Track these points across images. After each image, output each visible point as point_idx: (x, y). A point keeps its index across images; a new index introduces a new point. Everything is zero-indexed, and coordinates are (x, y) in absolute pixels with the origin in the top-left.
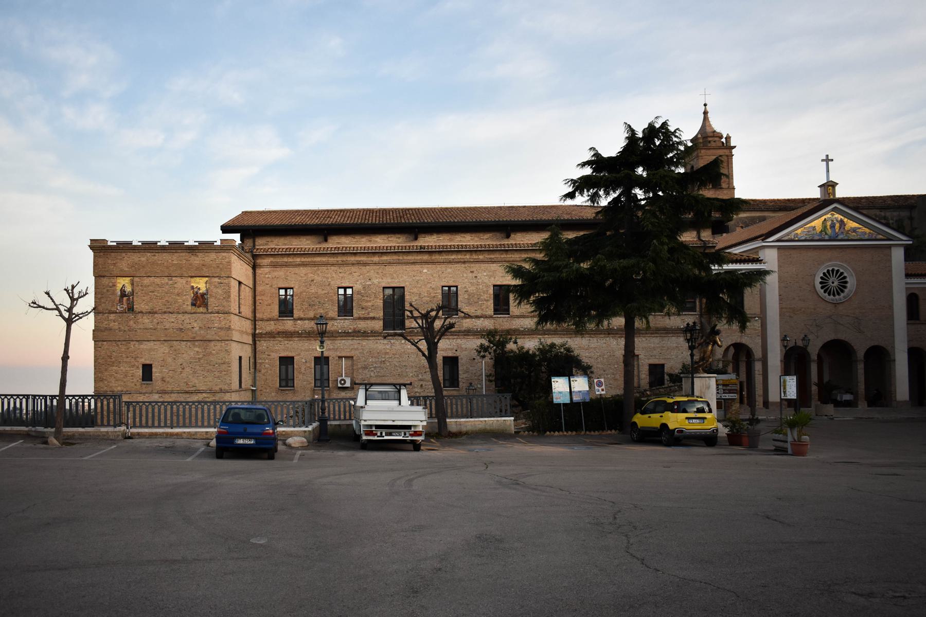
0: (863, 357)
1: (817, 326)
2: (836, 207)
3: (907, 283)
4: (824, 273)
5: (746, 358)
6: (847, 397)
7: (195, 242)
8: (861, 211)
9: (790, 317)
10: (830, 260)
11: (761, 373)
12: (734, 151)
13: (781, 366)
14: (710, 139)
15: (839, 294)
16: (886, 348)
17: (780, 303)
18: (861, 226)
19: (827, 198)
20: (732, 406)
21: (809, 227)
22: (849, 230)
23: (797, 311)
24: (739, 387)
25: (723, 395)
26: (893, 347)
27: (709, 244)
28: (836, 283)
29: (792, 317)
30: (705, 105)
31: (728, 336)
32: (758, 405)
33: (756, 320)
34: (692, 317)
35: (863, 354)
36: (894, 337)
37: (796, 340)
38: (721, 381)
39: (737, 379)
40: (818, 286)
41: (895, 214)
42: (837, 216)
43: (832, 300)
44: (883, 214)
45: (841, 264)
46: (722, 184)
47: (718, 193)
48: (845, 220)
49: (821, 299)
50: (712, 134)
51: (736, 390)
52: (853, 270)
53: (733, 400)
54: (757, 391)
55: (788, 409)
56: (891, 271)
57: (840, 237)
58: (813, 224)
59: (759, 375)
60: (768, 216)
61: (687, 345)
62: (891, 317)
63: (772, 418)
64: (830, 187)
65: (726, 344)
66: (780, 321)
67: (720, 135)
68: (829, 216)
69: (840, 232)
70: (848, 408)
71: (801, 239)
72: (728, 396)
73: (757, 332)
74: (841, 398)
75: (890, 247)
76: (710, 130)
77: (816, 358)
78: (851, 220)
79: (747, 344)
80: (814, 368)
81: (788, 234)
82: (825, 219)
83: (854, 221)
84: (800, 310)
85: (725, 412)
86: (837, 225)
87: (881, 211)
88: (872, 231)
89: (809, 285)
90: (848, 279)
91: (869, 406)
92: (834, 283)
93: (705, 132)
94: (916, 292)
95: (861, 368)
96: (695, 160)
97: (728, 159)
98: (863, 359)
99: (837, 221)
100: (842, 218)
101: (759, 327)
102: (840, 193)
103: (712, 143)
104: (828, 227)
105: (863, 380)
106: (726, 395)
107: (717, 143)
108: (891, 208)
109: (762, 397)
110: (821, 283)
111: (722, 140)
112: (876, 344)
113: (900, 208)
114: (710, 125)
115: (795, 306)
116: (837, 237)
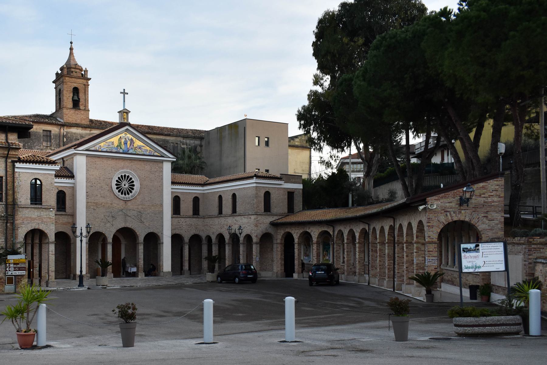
1: (112, 217)
2: (127, 129)
4: (119, 178)
5: (39, 241)
6: (134, 270)
7: (256, 169)
8: (147, 135)
9: (94, 209)
10: (123, 168)
11: (54, 253)
12: (90, 82)
13: (86, 247)
14: (73, 70)
15: (128, 194)
16: (158, 234)
17: (86, 199)
18: (144, 145)
19: (122, 121)
20: (21, 281)
21: (109, 142)
22: (136, 147)
23: (99, 205)
24: (27, 265)
25: (14, 272)
26: (162, 234)
27: (13, 146)
28: (127, 186)
29: (95, 210)
30: (71, 43)
31: (28, 223)
32: (51, 279)
33: (51, 211)
35: (143, 239)
36: (163, 226)
38: (12, 260)
39: (26, 258)
40: (114, 187)
41: (192, 142)
43: (124, 198)
44: (184, 141)
46: (80, 106)
47: (78, 112)
48: (134, 139)
49: (116, 197)
50: (74, 66)
51: (25, 268)
53: (22, 276)
55: (90, 280)
56: (162, 179)
57: (130, 151)
58: (112, 140)
59: (52, 254)
62: (161, 213)
63: (61, 289)
64: (125, 114)
66: (86, 212)
67: (80, 68)
68: (123, 135)
69: (131, 148)
70: (132, 278)
71: (103, 150)
72: (18, 273)
73: (51, 220)
74: (131, 270)
75: (162, 162)
76: (74, 63)
77: (111, 241)
78: (138, 140)
79: (44, 230)
80: (110, 248)
81: (94, 146)
83: (140, 141)
84: (101, 204)
85: (15, 286)
86: (129, 143)
87: (184, 139)
88: (151, 149)
90: (134, 183)
91: (146, 275)
92: (125, 185)
93: (70, 64)
95: (141, 248)
96: (62, 84)
97: (85, 87)
99: (129, 139)
100: (133, 137)
101: (53, 217)
102: (133, 119)
103: (74, 73)
104: (123, 143)
105: (143, 257)
106: (16, 272)
107: (78, 73)
108: (190, 138)
109: (54, 272)
110: (116, 185)
111: (82, 72)
112: (152, 231)
113: (195, 138)
114: (74, 59)
116: (128, 151)
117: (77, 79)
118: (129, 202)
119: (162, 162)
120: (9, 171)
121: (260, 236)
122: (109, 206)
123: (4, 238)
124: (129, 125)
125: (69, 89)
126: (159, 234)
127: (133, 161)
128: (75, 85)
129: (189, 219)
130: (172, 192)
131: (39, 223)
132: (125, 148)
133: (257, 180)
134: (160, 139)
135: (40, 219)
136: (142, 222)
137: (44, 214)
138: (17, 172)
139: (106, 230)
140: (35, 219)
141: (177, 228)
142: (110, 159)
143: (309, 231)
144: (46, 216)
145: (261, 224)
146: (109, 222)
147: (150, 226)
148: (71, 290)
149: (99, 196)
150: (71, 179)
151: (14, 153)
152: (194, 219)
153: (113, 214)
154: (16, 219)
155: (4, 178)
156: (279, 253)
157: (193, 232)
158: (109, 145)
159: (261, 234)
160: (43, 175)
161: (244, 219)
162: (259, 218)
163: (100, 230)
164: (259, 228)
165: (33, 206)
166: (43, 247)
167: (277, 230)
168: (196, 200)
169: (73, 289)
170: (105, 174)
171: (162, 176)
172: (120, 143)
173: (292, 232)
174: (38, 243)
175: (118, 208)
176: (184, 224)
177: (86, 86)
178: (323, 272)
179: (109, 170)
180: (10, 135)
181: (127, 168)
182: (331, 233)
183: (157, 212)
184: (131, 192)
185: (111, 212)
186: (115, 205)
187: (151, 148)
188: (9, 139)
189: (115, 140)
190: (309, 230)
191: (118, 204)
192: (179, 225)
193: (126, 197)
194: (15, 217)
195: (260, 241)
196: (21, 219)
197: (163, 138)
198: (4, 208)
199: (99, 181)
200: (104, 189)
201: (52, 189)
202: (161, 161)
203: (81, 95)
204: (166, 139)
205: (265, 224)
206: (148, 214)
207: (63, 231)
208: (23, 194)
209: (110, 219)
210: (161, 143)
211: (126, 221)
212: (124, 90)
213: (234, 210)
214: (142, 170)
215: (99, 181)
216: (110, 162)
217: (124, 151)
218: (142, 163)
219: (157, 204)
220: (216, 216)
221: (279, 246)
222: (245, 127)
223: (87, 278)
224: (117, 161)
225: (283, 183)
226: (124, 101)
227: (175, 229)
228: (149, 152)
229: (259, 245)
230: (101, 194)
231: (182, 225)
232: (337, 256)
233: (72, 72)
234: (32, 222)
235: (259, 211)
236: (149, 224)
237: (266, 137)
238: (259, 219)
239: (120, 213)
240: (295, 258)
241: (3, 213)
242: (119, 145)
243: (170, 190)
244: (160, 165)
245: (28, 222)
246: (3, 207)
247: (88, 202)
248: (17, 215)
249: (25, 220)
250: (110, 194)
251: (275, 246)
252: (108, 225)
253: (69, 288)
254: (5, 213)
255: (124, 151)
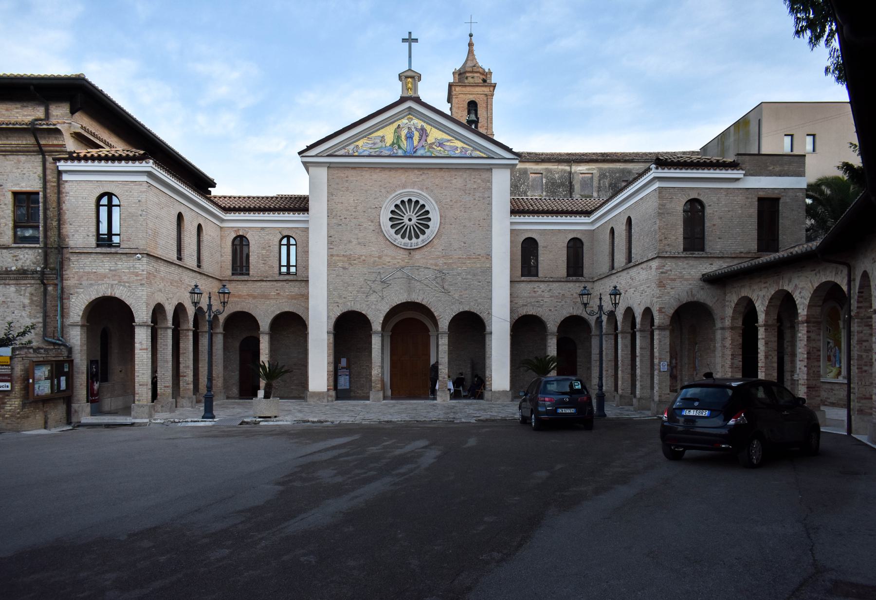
0: (447, 328)
2: (410, 108)
3: (512, 223)
9: (344, 268)
13: (328, 340)
15: (417, 237)
16: (481, 315)
17: (329, 248)
18: (450, 138)
20: (5, 403)
22: (433, 143)
23: (355, 260)
26: (490, 314)
29: (347, 269)
30: (471, 35)
31: (91, 284)
34: (30, 252)
37: (210, 293)
40: (386, 224)
42: (415, 121)
43: (405, 244)
45: (420, 192)
48: (426, 126)
52: (436, 202)
54: (138, 376)
57: (420, 152)
60: (530, 168)
61: (194, 309)
62: (488, 271)
64: (409, 80)
65: (88, 297)
67: (481, 70)
68: (405, 121)
71: (362, 154)
73: (139, 278)
82: (399, 125)
86: (416, 135)
89: (372, 222)
92: (410, 218)
94: (534, 236)
98: (447, 331)
99: (416, 129)
104: (403, 138)
112: (466, 309)
115: (352, 253)
116: (415, 152)
117: (474, 88)
118: (417, 251)
119: (489, 169)
120: (52, 180)
121: (672, 311)
122: (374, 262)
123: (42, 315)
124: (417, 100)
125: (462, 106)
126: (483, 316)
127: (426, 172)
128: (471, 98)
129: (557, 284)
130: (511, 230)
131: (112, 285)
132: (408, 148)
133: (660, 170)
134: (616, 169)
135: (115, 275)
136: (447, 292)
137: (123, 265)
138: (66, 181)
139: (369, 308)
140: (105, 276)
141: (531, 303)
142: (378, 171)
143: (789, 288)
144: (127, 271)
145: (674, 280)
146: (375, 292)
147: (462, 298)
148: (179, 424)
149: (355, 242)
150: (303, 214)
151: (55, 142)
152: (571, 285)
153: (382, 276)
154: (65, 277)
155: (41, 194)
156: (728, 352)
157: (566, 313)
158: (374, 144)
159: (676, 305)
160: (120, 186)
161: (641, 271)
162: (669, 265)
163: (357, 308)
164: (668, 289)
165: (99, 250)
166: (159, 336)
167: (725, 294)
168: (575, 247)
169: (184, 424)
170: (367, 200)
171: (490, 197)
172: (399, 138)
173: (754, 297)
174: (221, 333)
175: (395, 264)
176: (546, 294)
177: (489, 97)
178: (706, 413)
179: (375, 191)
180: (54, 107)
181: (414, 184)
182: (845, 288)
183: (479, 270)
184: (423, 233)
185: (379, 272)
186: (388, 259)
187: (464, 143)
188: (53, 116)
189: (388, 134)
190: (790, 286)
191: (394, 258)
192: (535, 297)
193: (411, 244)
194: (64, 273)
195: (670, 323)
196: (76, 278)
197: (621, 167)
198: (42, 254)
199: (353, 213)
200: (365, 228)
201: (140, 213)
202: (488, 167)
203: (481, 112)
204: (626, 168)
205: (687, 280)
206: (459, 274)
207: (291, 311)
208: (80, 226)
209: (377, 287)
210: (618, 175)
211: (410, 290)
212: (410, 33)
213: (629, 259)
214: (446, 187)
215: (353, 213)
216: (377, 176)
217: (405, 152)
218: (446, 175)
219: (479, 255)
220: (606, 275)
221: (728, 334)
222: (759, 120)
223: (330, 399)
224: (392, 173)
225: (742, 176)
226: (410, 57)
227: (526, 305)
228: (461, 152)
229: (667, 333)
230: (357, 239)
231: (541, 296)
232: (860, 357)
233: (467, 78)
234: (99, 282)
235: (667, 249)
236: (460, 295)
237: (808, 135)
238: (667, 268)
239: (399, 274)
240: (760, 365)
241: (38, 265)
242: (395, 142)
243: (507, 228)
244: (485, 175)
245: (90, 282)
246: (39, 253)
247: (332, 255)
248: (69, 268)
249: (85, 278)
250: (377, 239)
251: (719, 335)
252: (373, 298)
253: (177, 420)
254: (42, 266)
255: (405, 152)
